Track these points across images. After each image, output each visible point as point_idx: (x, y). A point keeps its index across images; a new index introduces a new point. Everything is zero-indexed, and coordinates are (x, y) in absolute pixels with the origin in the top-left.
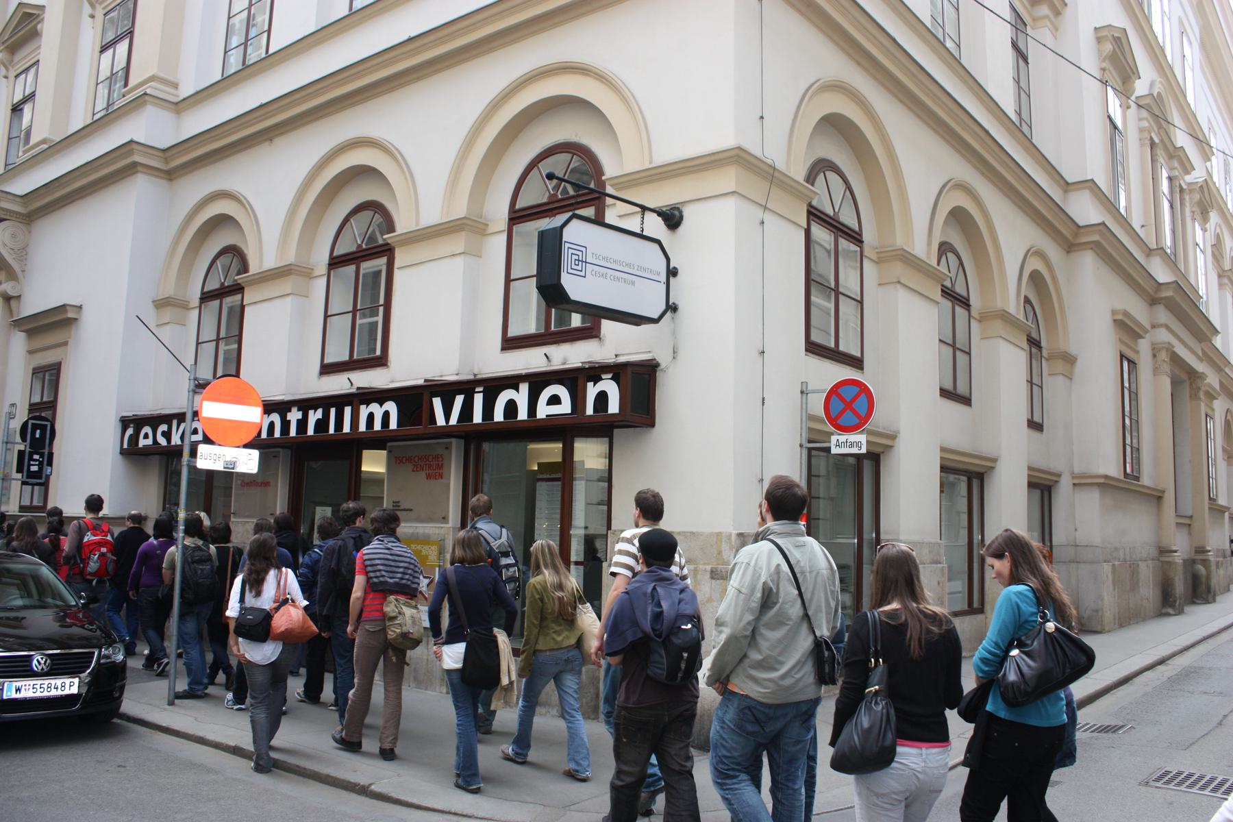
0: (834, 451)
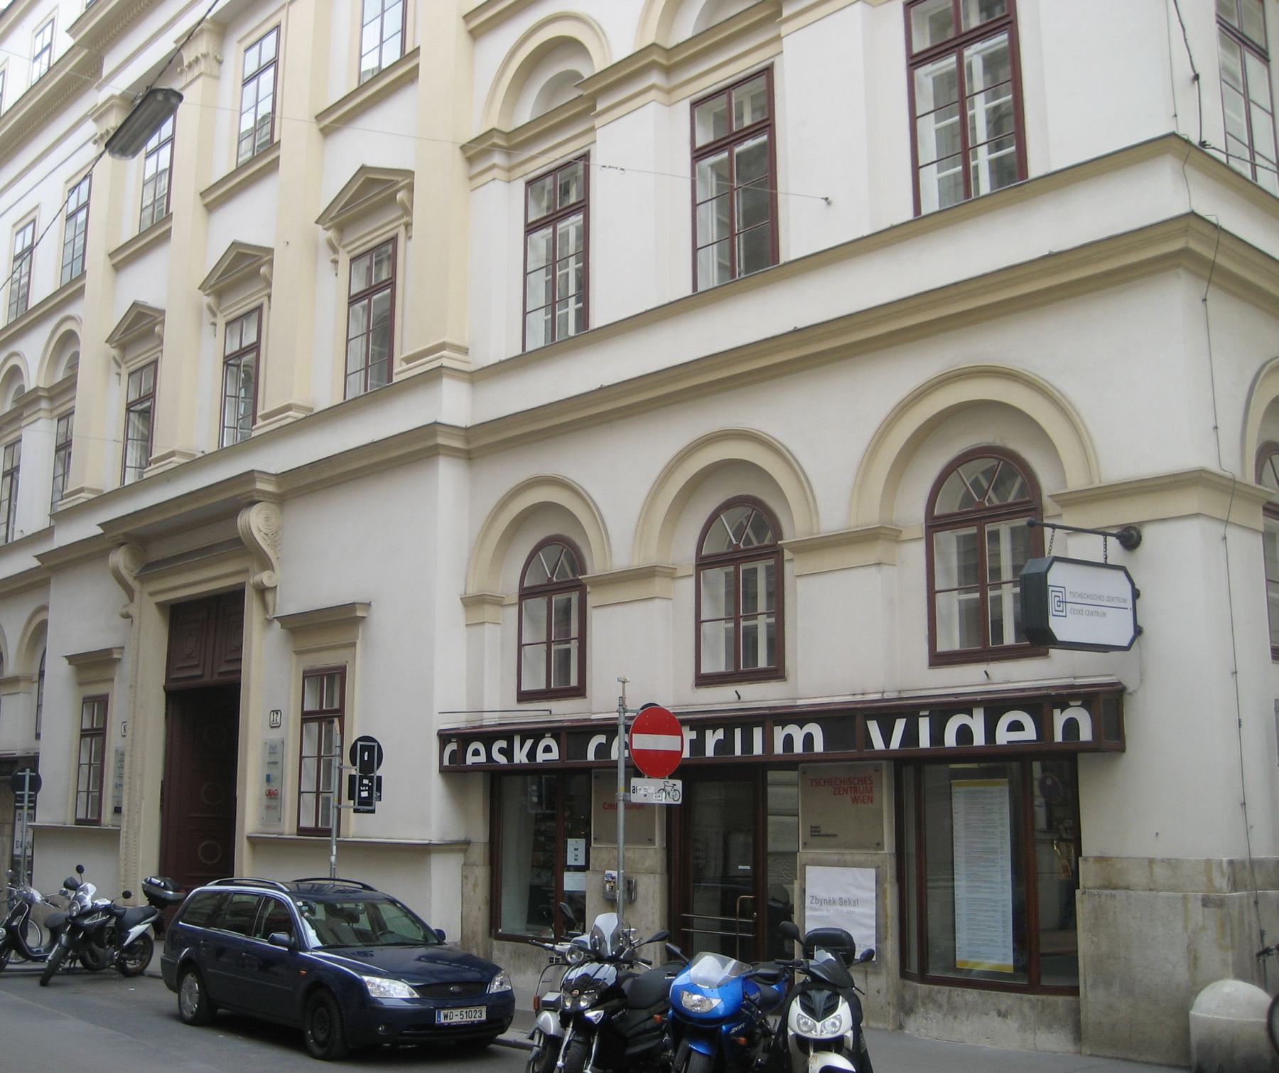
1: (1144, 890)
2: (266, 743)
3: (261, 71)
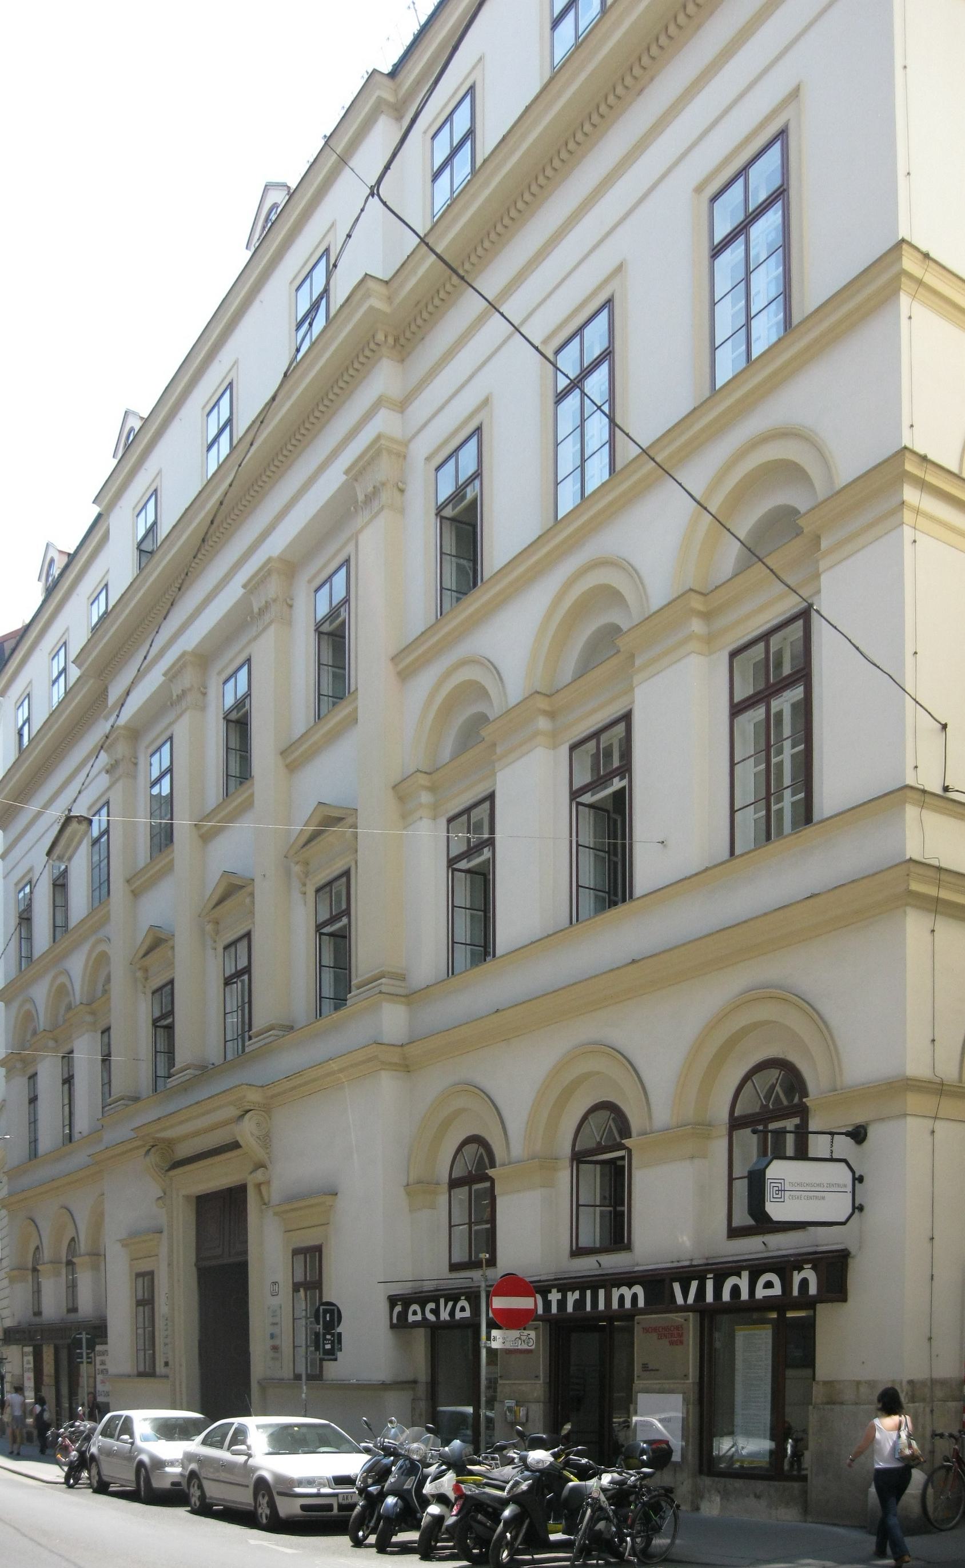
1: (852, 1404)
2: (269, 1308)
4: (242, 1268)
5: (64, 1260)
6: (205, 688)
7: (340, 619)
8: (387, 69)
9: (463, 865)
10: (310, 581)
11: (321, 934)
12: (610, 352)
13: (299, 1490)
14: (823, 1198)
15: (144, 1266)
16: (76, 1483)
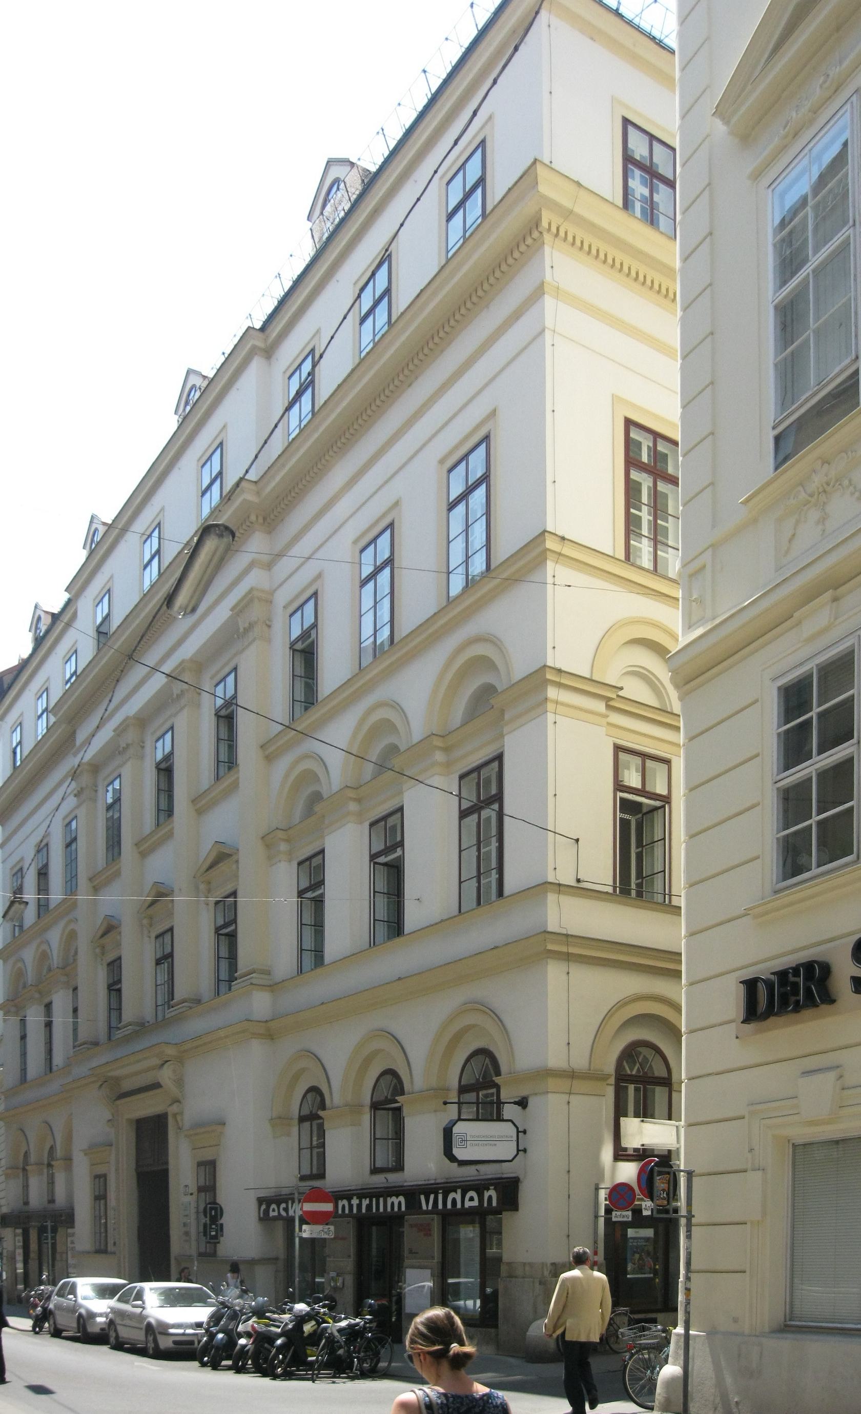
0: (614, 1219)
3: (378, 570)
4: (165, 1173)
5: (46, 1162)
6: (143, 743)
7: (311, 640)
8: (258, 325)
9: (382, 859)
10: (212, 678)
11: (219, 935)
12: (487, 476)
13: (172, 1331)
14: (495, 1145)
15: (101, 1170)
16: (41, 1330)
